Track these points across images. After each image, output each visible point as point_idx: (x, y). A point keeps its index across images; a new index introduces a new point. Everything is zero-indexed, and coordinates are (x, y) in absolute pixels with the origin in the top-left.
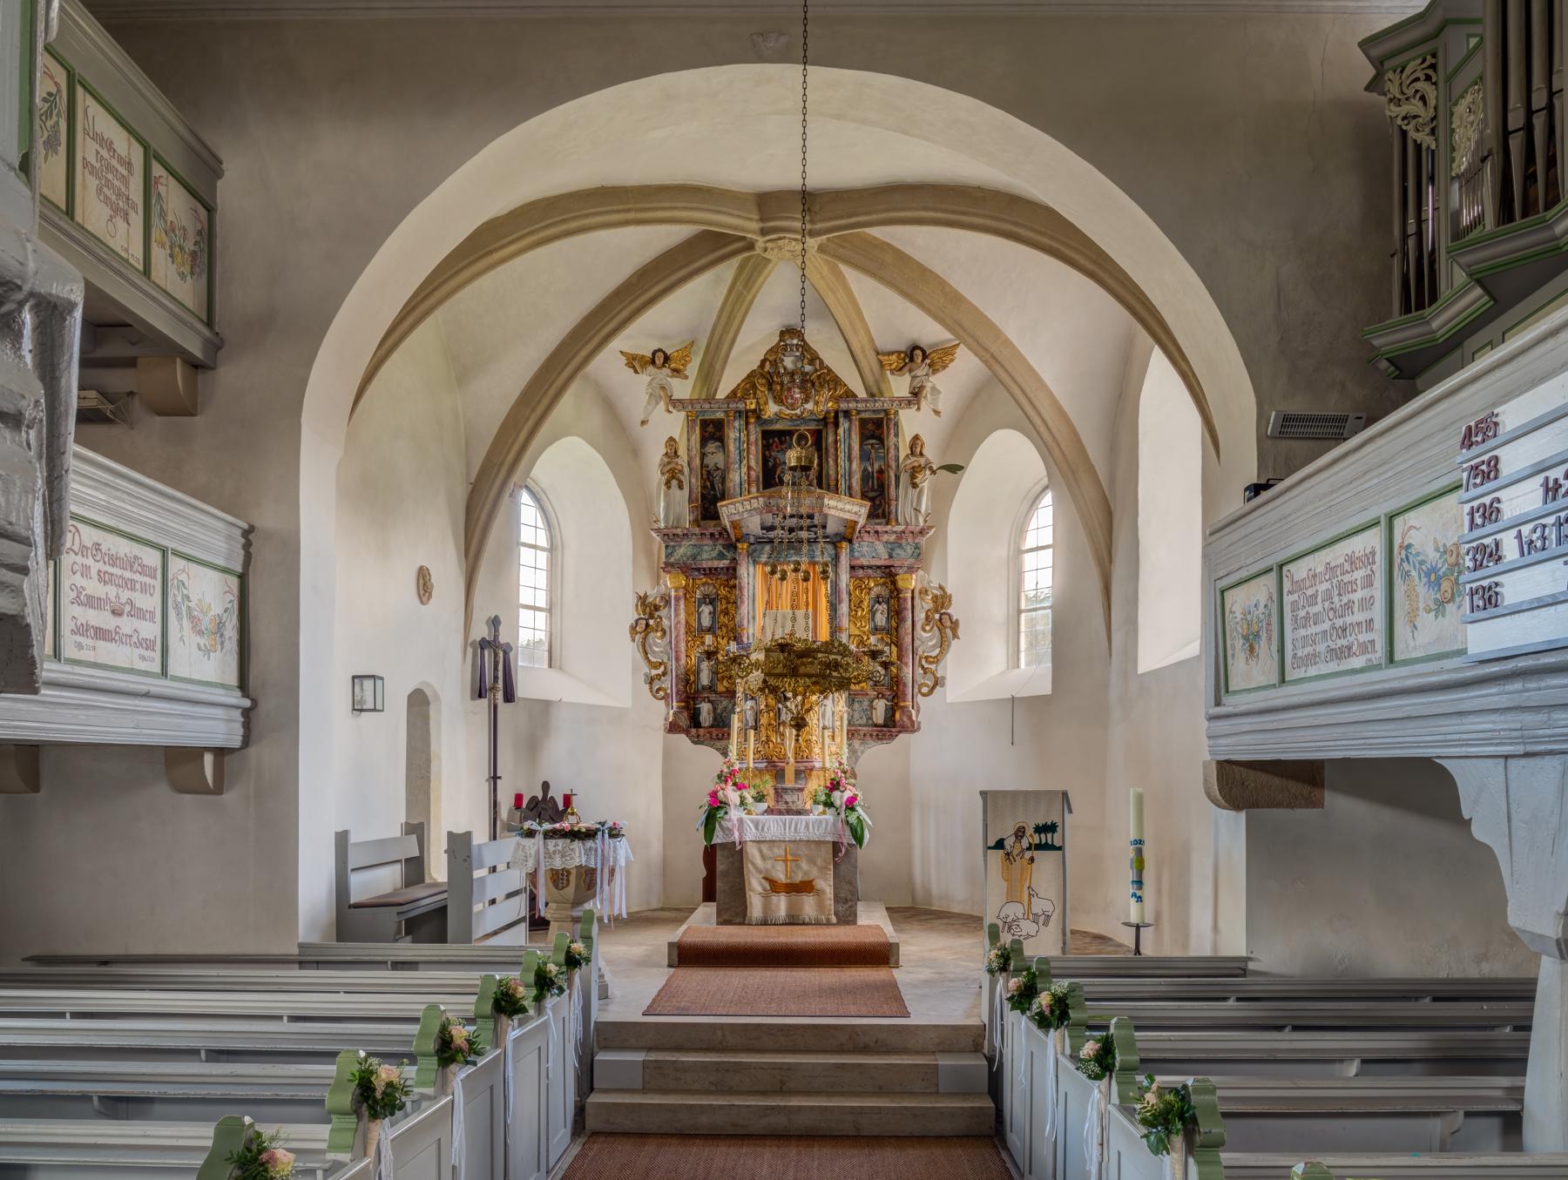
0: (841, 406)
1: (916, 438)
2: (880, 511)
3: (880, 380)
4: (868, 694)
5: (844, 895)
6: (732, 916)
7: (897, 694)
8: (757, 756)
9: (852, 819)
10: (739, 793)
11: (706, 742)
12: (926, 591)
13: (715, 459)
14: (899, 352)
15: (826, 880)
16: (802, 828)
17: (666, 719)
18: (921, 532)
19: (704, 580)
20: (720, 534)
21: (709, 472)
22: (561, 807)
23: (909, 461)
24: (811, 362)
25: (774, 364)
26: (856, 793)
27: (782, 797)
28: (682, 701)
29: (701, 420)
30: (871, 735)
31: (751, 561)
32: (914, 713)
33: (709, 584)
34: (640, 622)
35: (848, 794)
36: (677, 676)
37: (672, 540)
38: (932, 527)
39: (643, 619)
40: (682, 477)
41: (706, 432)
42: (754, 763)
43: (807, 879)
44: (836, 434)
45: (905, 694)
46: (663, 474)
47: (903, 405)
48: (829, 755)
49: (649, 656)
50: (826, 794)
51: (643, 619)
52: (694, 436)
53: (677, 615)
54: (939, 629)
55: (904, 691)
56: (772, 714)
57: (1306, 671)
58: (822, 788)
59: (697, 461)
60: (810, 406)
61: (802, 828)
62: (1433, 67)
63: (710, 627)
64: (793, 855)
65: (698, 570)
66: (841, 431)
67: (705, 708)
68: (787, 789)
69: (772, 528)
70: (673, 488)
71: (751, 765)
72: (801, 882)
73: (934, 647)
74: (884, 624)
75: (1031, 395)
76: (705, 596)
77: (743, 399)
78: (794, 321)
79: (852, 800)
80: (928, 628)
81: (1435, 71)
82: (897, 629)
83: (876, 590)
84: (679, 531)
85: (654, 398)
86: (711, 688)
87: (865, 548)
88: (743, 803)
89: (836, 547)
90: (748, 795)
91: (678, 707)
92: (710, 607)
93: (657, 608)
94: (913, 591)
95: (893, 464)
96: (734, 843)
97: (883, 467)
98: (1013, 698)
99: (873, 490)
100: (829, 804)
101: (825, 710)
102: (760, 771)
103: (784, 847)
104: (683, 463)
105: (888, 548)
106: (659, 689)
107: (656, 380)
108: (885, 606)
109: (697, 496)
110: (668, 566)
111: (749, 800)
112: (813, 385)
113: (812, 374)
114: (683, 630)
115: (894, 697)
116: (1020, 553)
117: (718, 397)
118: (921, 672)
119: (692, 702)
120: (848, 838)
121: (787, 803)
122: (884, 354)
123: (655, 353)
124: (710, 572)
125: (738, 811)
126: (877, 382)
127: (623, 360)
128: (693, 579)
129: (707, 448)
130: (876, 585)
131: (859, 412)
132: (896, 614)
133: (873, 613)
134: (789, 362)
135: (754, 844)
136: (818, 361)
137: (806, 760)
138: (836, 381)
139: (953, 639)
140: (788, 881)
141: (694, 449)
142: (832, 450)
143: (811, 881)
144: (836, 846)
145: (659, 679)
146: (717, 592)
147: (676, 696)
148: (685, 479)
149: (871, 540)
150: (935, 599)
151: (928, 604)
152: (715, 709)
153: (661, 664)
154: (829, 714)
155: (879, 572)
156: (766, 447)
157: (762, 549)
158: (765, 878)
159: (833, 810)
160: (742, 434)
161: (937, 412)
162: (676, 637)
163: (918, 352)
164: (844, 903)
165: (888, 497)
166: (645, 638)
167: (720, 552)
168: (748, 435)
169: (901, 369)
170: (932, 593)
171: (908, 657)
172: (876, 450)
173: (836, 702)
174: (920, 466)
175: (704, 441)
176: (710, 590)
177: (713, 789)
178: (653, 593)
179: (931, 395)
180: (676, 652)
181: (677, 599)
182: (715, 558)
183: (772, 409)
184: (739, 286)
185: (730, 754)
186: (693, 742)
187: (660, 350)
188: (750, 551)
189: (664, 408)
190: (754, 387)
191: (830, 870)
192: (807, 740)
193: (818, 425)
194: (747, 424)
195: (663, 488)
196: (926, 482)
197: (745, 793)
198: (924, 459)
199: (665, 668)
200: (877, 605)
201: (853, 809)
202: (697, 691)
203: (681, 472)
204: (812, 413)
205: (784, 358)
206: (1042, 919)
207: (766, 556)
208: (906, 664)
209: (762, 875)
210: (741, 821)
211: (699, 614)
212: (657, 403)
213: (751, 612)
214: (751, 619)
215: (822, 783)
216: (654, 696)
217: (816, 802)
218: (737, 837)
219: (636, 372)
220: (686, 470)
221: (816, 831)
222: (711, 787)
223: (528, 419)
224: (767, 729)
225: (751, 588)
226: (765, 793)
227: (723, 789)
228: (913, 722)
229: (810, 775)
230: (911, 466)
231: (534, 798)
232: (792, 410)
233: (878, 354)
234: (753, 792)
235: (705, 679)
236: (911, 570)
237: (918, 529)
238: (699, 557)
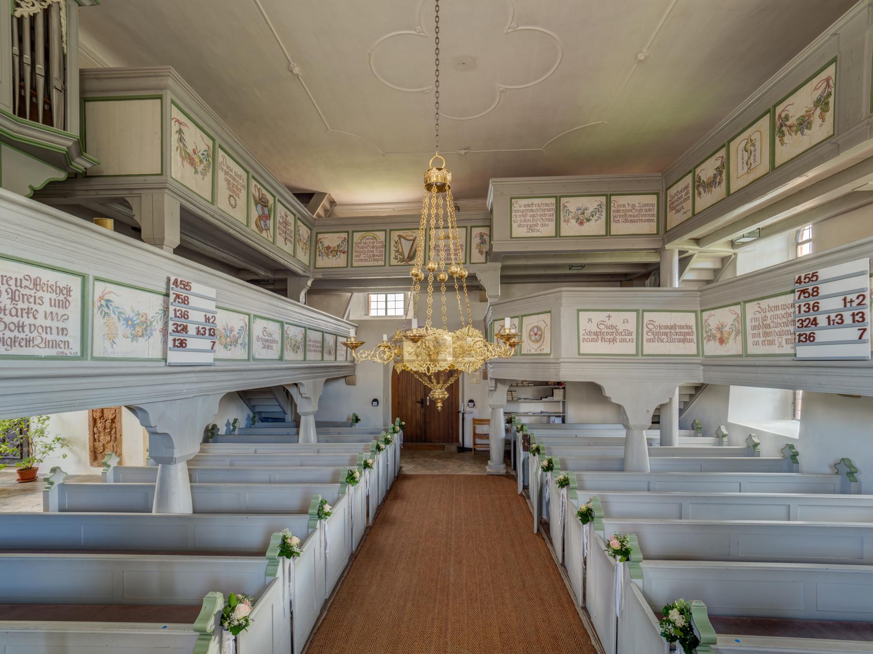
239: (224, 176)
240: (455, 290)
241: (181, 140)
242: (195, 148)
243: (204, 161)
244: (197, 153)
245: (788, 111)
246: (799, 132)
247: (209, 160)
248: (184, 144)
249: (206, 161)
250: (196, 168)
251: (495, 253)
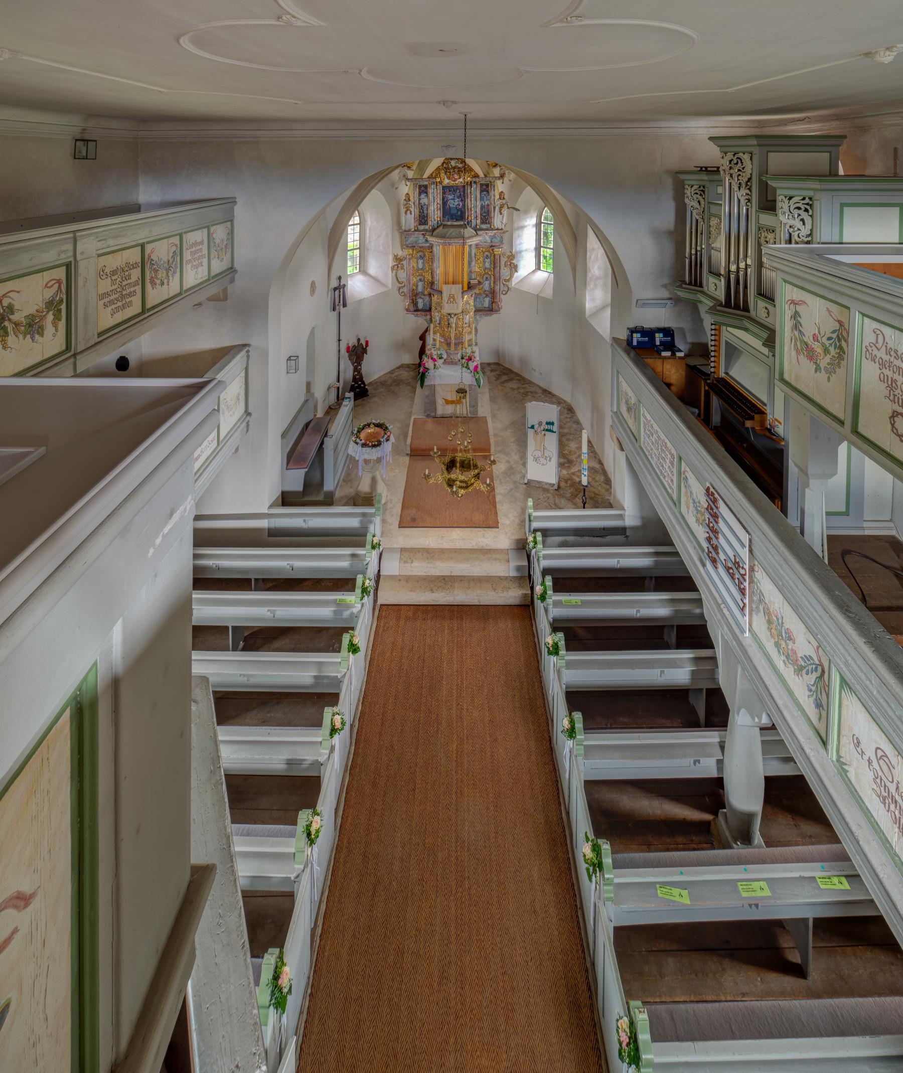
13: (424, 200)
21: (422, 206)
22: (364, 345)
35: (475, 364)
45: (496, 297)
60: (461, 180)
62: (703, 191)
77: (435, 178)
81: (704, 193)
92: (422, 261)
95: (493, 202)
99: (485, 212)
132: (494, 263)
133: (484, 262)
138: (471, 170)
142: (469, 196)
148: (412, 210)
156: (444, 193)
175: (420, 194)
178: (400, 254)
206: (548, 458)
208: (497, 285)
220: (413, 206)
239: (879, 372)
240: (433, 458)
241: (797, 326)
242: (817, 332)
243: (832, 349)
244: (819, 338)
245: (13, 299)
246: (29, 336)
247: (840, 345)
248: (800, 331)
249: (835, 349)
250: (818, 362)
251: (277, 947)
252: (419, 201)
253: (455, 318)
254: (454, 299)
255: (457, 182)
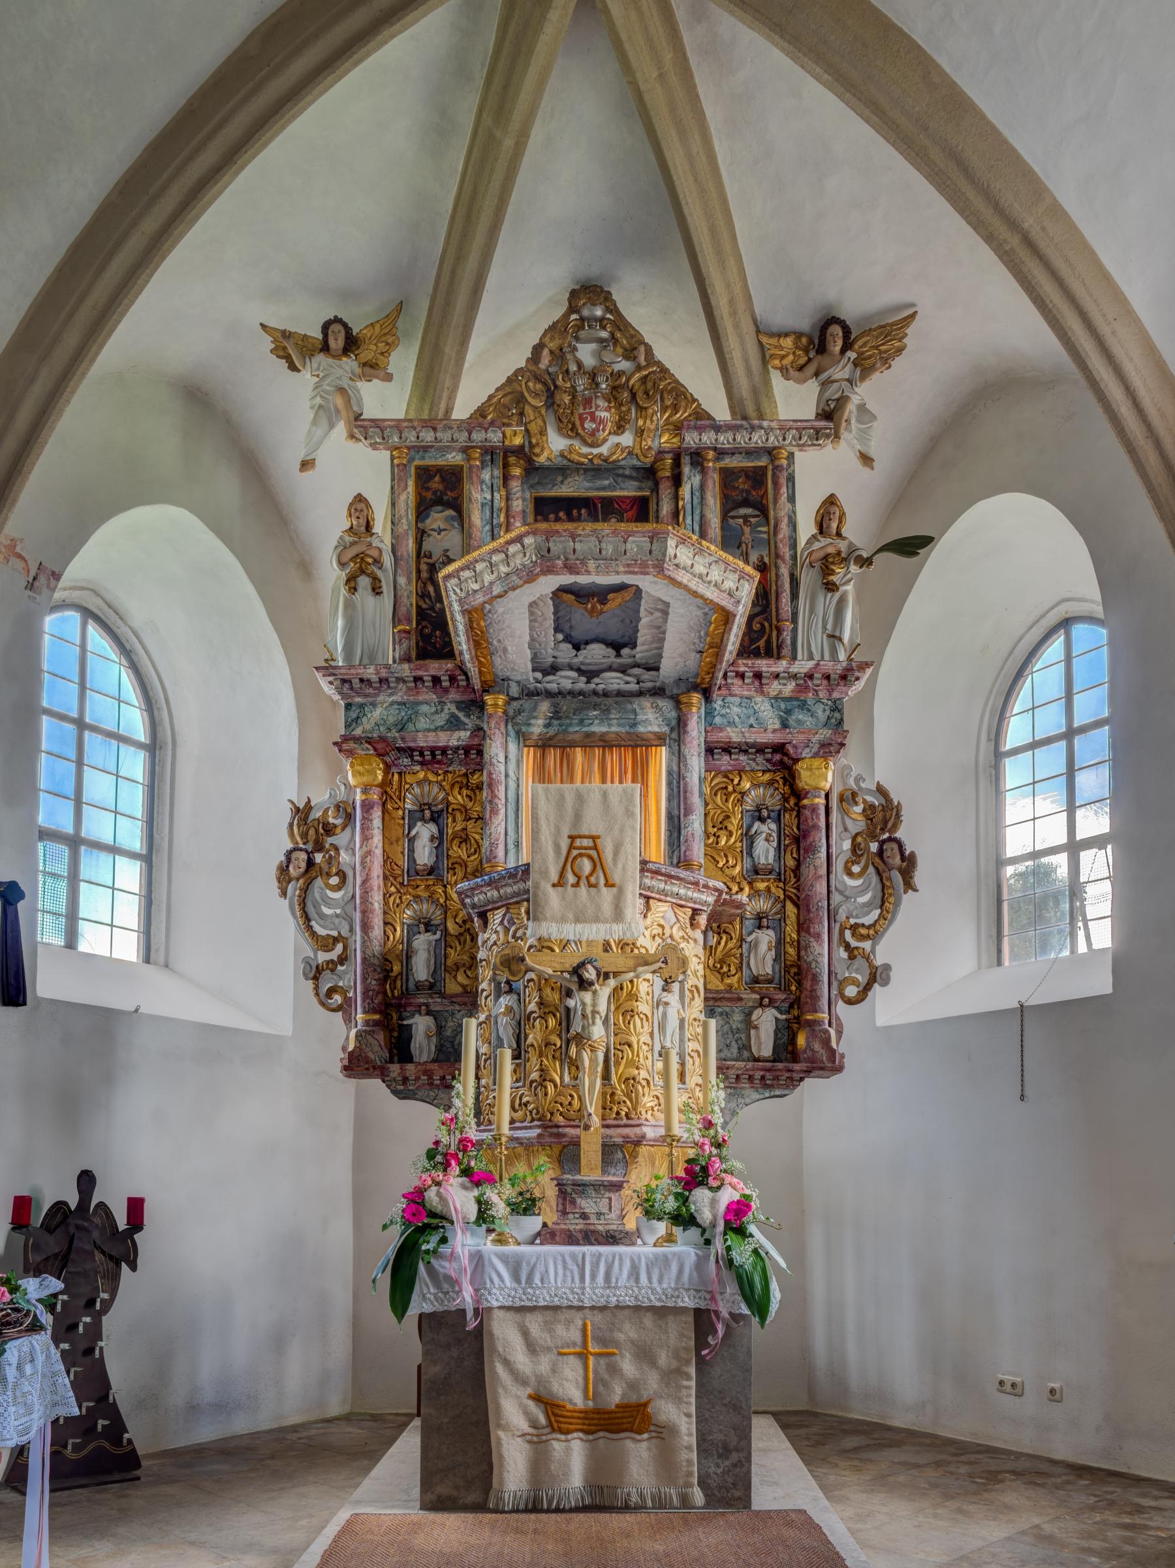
0: (688, 438)
1: (831, 501)
2: (762, 643)
3: (762, 391)
4: (740, 999)
5: (721, 1437)
6: (457, 1488)
7: (798, 999)
8: (520, 1113)
9: (742, 1255)
10: (476, 1193)
11: (420, 1094)
12: (854, 795)
14: (799, 335)
15: (678, 1401)
16: (622, 1276)
17: (344, 1049)
18: (844, 677)
19: (421, 775)
20: (452, 679)
22: (122, 1223)
23: (817, 545)
24: (629, 354)
25: (559, 356)
26: (748, 1192)
27: (573, 1202)
28: (375, 1011)
29: (418, 468)
30: (751, 1078)
31: (512, 733)
32: (832, 1032)
33: (430, 782)
34: (295, 855)
35: (727, 1196)
36: (364, 960)
37: (358, 694)
38: (864, 666)
39: (301, 850)
40: (379, 573)
41: (428, 489)
42: (510, 1129)
43: (633, 1398)
44: (676, 498)
45: (815, 998)
46: (342, 565)
47: (804, 439)
48: (680, 1111)
49: (313, 923)
50: (677, 1196)
51: (301, 850)
52: (403, 497)
53: (366, 838)
54: (877, 869)
55: (813, 991)
56: (552, 1022)
57: (10, 1365)
58: (666, 1181)
59: (410, 544)
60: (627, 439)
61: (622, 1276)
63: (432, 867)
64: (601, 1341)
65: (409, 751)
66: (685, 491)
67: (421, 1025)
68: (584, 1185)
69: (554, 669)
70: (360, 589)
71: (505, 1129)
72: (617, 1406)
73: (868, 905)
74: (771, 860)
75: (1104, 329)
76: (422, 807)
78: (592, 270)
79: (739, 1209)
80: (856, 869)
82: (797, 871)
83: (755, 796)
84: (370, 673)
85: (324, 414)
86: (432, 987)
87: (736, 709)
88: (484, 1215)
89: (677, 702)
90: (498, 1199)
91: (367, 1023)
92: (433, 828)
93: (329, 830)
94: (827, 796)
95: (786, 551)
96: (462, 1312)
97: (766, 560)
98: (1022, 1006)
100: (684, 1219)
101: (665, 1014)
102: (527, 1145)
103: (580, 1323)
104: (381, 545)
105: (779, 709)
106: (331, 992)
107: (328, 380)
108: (774, 826)
109: (409, 612)
110: (345, 744)
111: (500, 1209)
112: (634, 396)
113: (633, 374)
114: (377, 870)
115: (791, 1006)
116: (998, 756)
117: (455, 415)
118: (844, 955)
119: (395, 1016)
120: (730, 1302)
121: (584, 1216)
122: (771, 335)
123: (326, 327)
124: (434, 757)
125: (473, 1234)
126: (755, 392)
127: (267, 343)
128: (400, 774)
129: (428, 521)
130: (755, 786)
131: (721, 453)
133: (749, 839)
134: (586, 353)
135: (510, 1315)
136: (642, 349)
137: (625, 1121)
138: (679, 395)
139: (905, 892)
140: (590, 1403)
141: (404, 521)
143: (645, 1405)
144: (703, 1320)
145: (333, 971)
146: (445, 799)
147: (363, 1001)
149: (746, 693)
150: (869, 809)
151: (856, 820)
152: (440, 1028)
153: (336, 940)
154: (673, 1024)
155: (760, 759)
157: (535, 708)
158: (537, 1398)
159: (693, 1232)
160: (495, 494)
161: (866, 460)
162: (364, 882)
163: (836, 330)
164: (720, 1456)
165: (777, 615)
166: (305, 890)
167: (453, 715)
168: (508, 499)
169: (801, 369)
170: (865, 801)
171: (821, 922)
172: (754, 527)
173: (687, 1000)
174: (839, 553)
175: (422, 510)
176: (435, 794)
177: (418, 1183)
178: (321, 798)
179: (859, 421)
180: (364, 912)
181: (367, 807)
182: (442, 728)
183: (556, 444)
184: (487, 120)
185: (457, 1102)
186: (395, 1092)
187: (337, 320)
188: (511, 713)
189: (345, 434)
190: (520, 400)
191: (689, 1378)
192: (627, 1079)
193: (640, 489)
194: (506, 478)
195: (343, 592)
196: (849, 579)
197: (491, 1194)
198: (846, 542)
199: (345, 948)
200: (757, 825)
201: (741, 1232)
202: (406, 993)
203: (377, 562)
204: (630, 453)
205: (578, 345)
207: (541, 722)
208: (818, 936)
209: (529, 1391)
210: (478, 1260)
211: (412, 840)
212: (332, 426)
213: (511, 832)
214: (511, 846)
215: (663, 1171)
216: (323, 1004)
217: (650, 1213)
218: (468, 1299)
219: (293, 367)
220: (387, 560)
221: (655, 1284)
222: (410, 1183)
223: (32, 380)
224: (541, 1055)
225: (512, 785)
226: (537, 1193)
227: (438, 1184)
228: (832, 1053)
229: (634, 1155)
230: (821, 554)
231: (59, 1207)
232: (592, 446)
233: (758, 331)
234: (509, 1191)
235: (421, 970)
236: (830, 749)
237: (839, 668)
238: (410, 726)
252: (419, 543)
253: (605, 992)
254: (598, 863)
255: (604, 450)
